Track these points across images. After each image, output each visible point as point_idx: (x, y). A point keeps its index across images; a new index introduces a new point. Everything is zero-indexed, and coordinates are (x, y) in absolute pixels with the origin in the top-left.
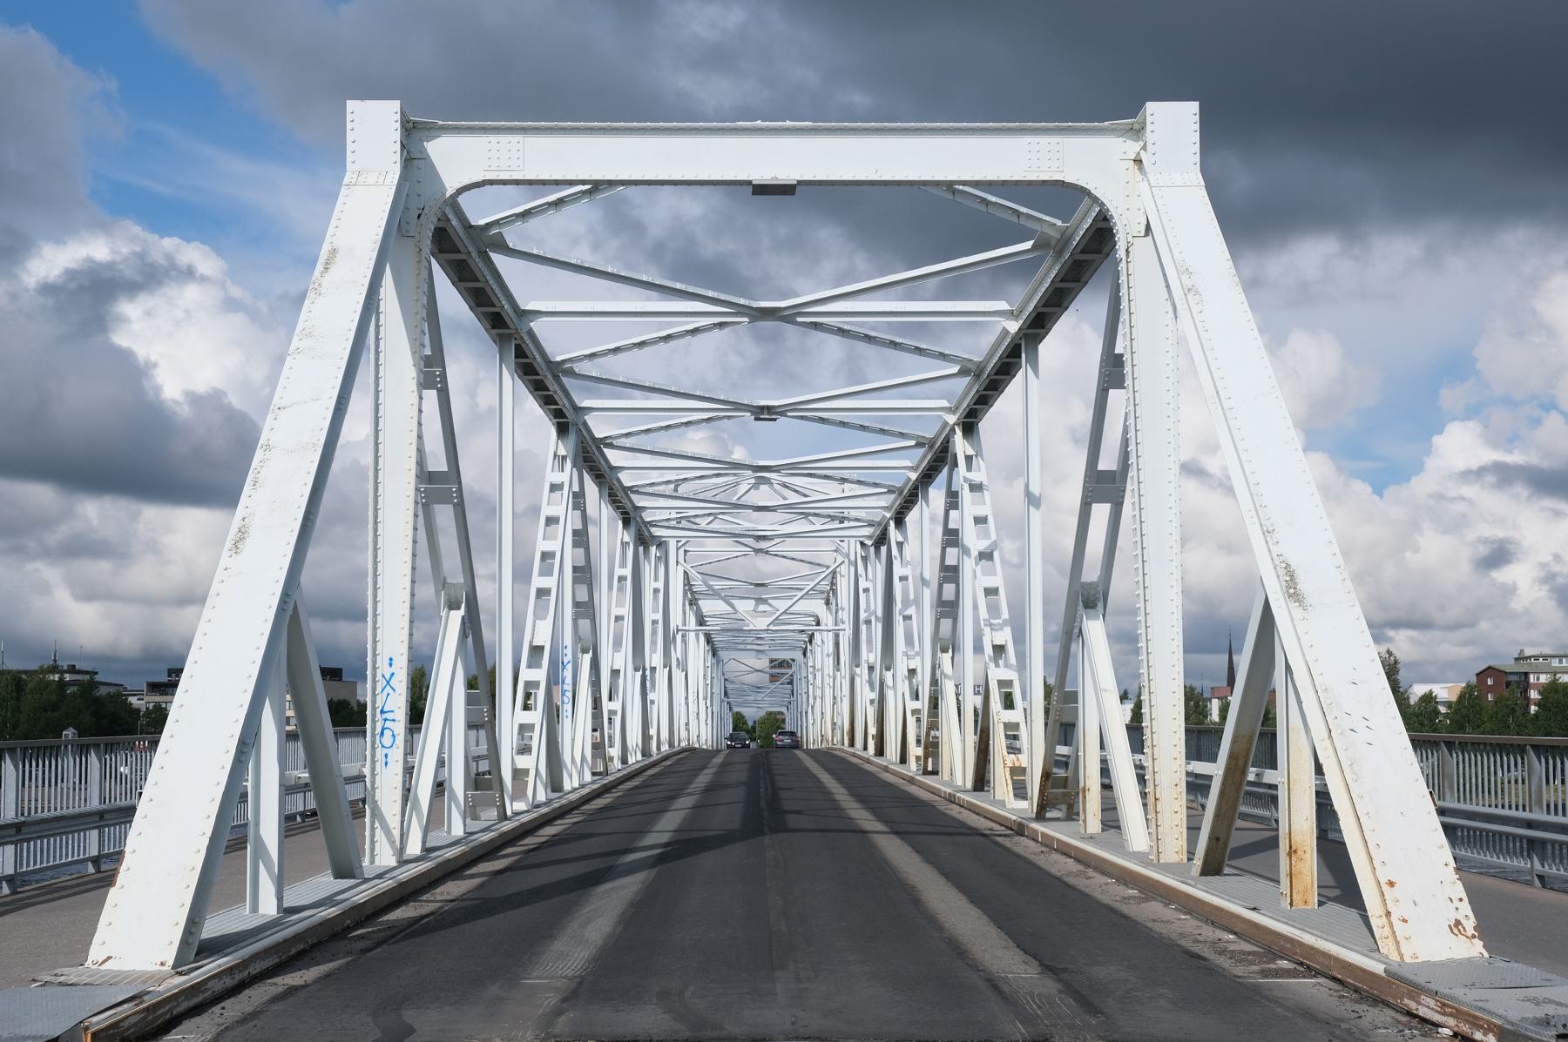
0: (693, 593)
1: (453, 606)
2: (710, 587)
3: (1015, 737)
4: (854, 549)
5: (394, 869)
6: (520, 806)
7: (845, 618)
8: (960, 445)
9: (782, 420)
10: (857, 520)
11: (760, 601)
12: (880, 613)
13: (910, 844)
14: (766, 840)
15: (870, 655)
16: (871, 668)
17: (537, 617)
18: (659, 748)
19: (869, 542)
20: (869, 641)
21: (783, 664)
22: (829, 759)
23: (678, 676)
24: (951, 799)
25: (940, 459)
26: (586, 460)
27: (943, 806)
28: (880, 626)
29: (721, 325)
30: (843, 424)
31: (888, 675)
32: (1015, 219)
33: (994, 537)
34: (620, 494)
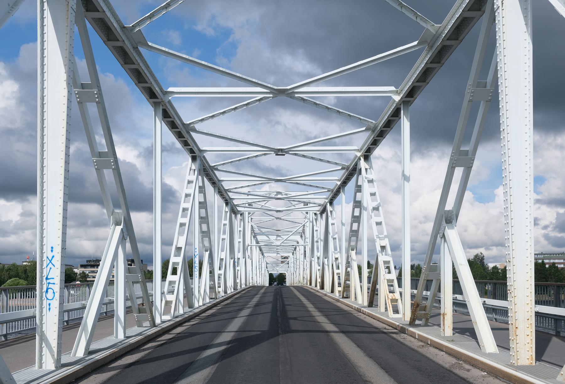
0: (254, 233)
1: (206, 251)
2: (261, 231)
3: (392, 286)
4: (311, 216)
5: (53, 371)
6: (167, 317)
7: (308, 241)
8: (363, 164)
9: (287, 155)
10: (315, 204)
11: (278, 236)
12: (322, 238)
13: (348, 337)
14: (280, 338)
15: (319, 253)
16: (318, 258)
17: (179, 234)
18: (241, 287)
19: (318, 213)
20: (318, 248)
21: (286, 258)
22: (301, 289)
23: (249, 262)
24: (359, 310)
25: (353, 172)
26: (205, 170)
27: (356, 314)
28: (322, 243)
29: (265, 154)
30: (304, 185)
31: (326, 260)
32: (414, 18)
33: (379, 201)
34: (224, 192)
